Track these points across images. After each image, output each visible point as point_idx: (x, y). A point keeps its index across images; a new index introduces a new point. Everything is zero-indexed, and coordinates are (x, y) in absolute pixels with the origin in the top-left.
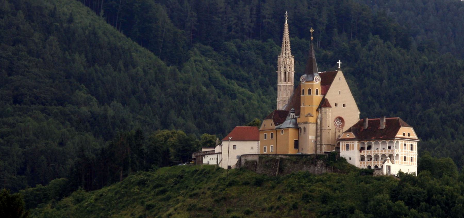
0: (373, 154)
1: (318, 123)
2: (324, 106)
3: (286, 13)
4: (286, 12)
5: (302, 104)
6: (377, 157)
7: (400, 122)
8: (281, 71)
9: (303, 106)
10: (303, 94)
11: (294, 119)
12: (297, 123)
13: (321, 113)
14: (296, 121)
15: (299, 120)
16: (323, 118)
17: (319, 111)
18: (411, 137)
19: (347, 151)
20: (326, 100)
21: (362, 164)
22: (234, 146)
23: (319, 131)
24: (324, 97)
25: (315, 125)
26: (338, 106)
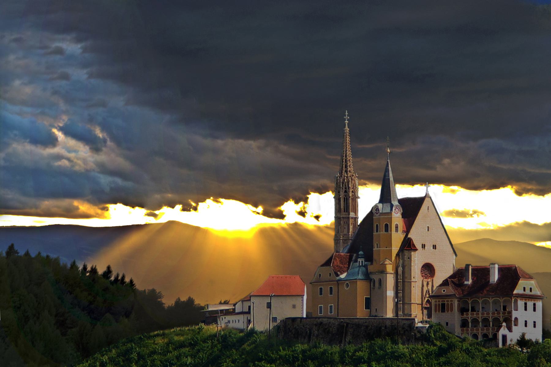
0: (470, 318)
1: (399, 273)
2: (407, 249)
3: (346, 112)
4: (346, 111)
5: (375, 245)
6: (486, 321)
7: (518, 272)
8: (340, 197)
9: (377, 249)
10: (377, 231)
11: (363, 266)
12: (368, 272)
13: (403, 259)
14: (367, 269)
15: (371, 268)
16: (407, 265)
17: (400, 256)
18: (533, 293)
19: (444, 314)
21: (465, 332)
22: (268, 304)
23: (400, 285)
24: (407, 235)
26: (426, 248)
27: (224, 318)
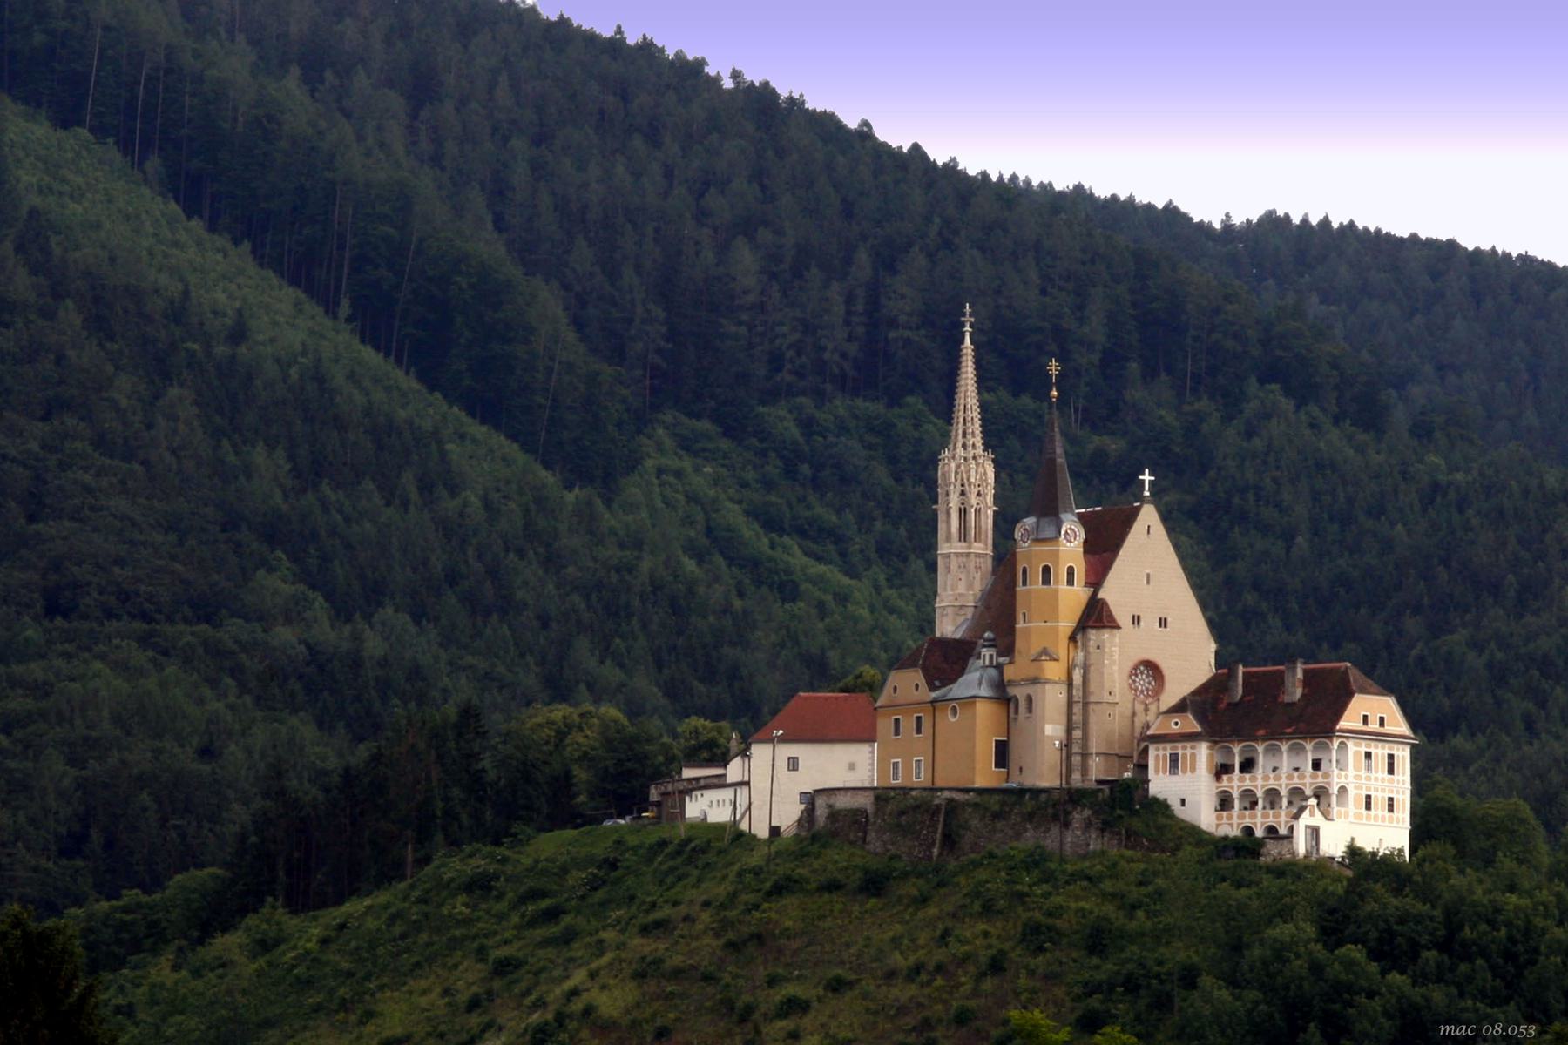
1: (1074, 682)
5: (1020, 617)
6: (1273, 796)
10: (1024, 583)
14: (1001, 674)
15: (1010, 673)
18: (1388, 729)
20: (1103, 603)
21: (1225, 820)
23: (1077, 709)
24: (1095, 594)
25: (1064, 688)
26: (1142, 623)
27: (699, 796)
